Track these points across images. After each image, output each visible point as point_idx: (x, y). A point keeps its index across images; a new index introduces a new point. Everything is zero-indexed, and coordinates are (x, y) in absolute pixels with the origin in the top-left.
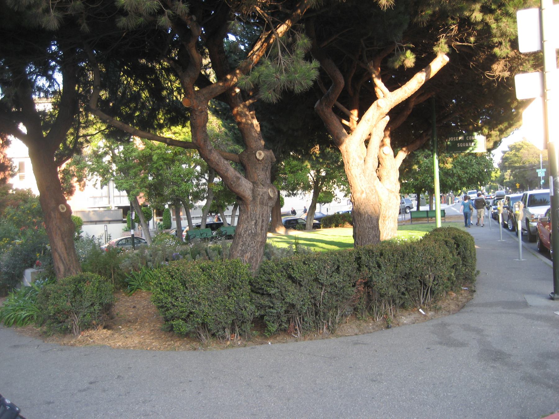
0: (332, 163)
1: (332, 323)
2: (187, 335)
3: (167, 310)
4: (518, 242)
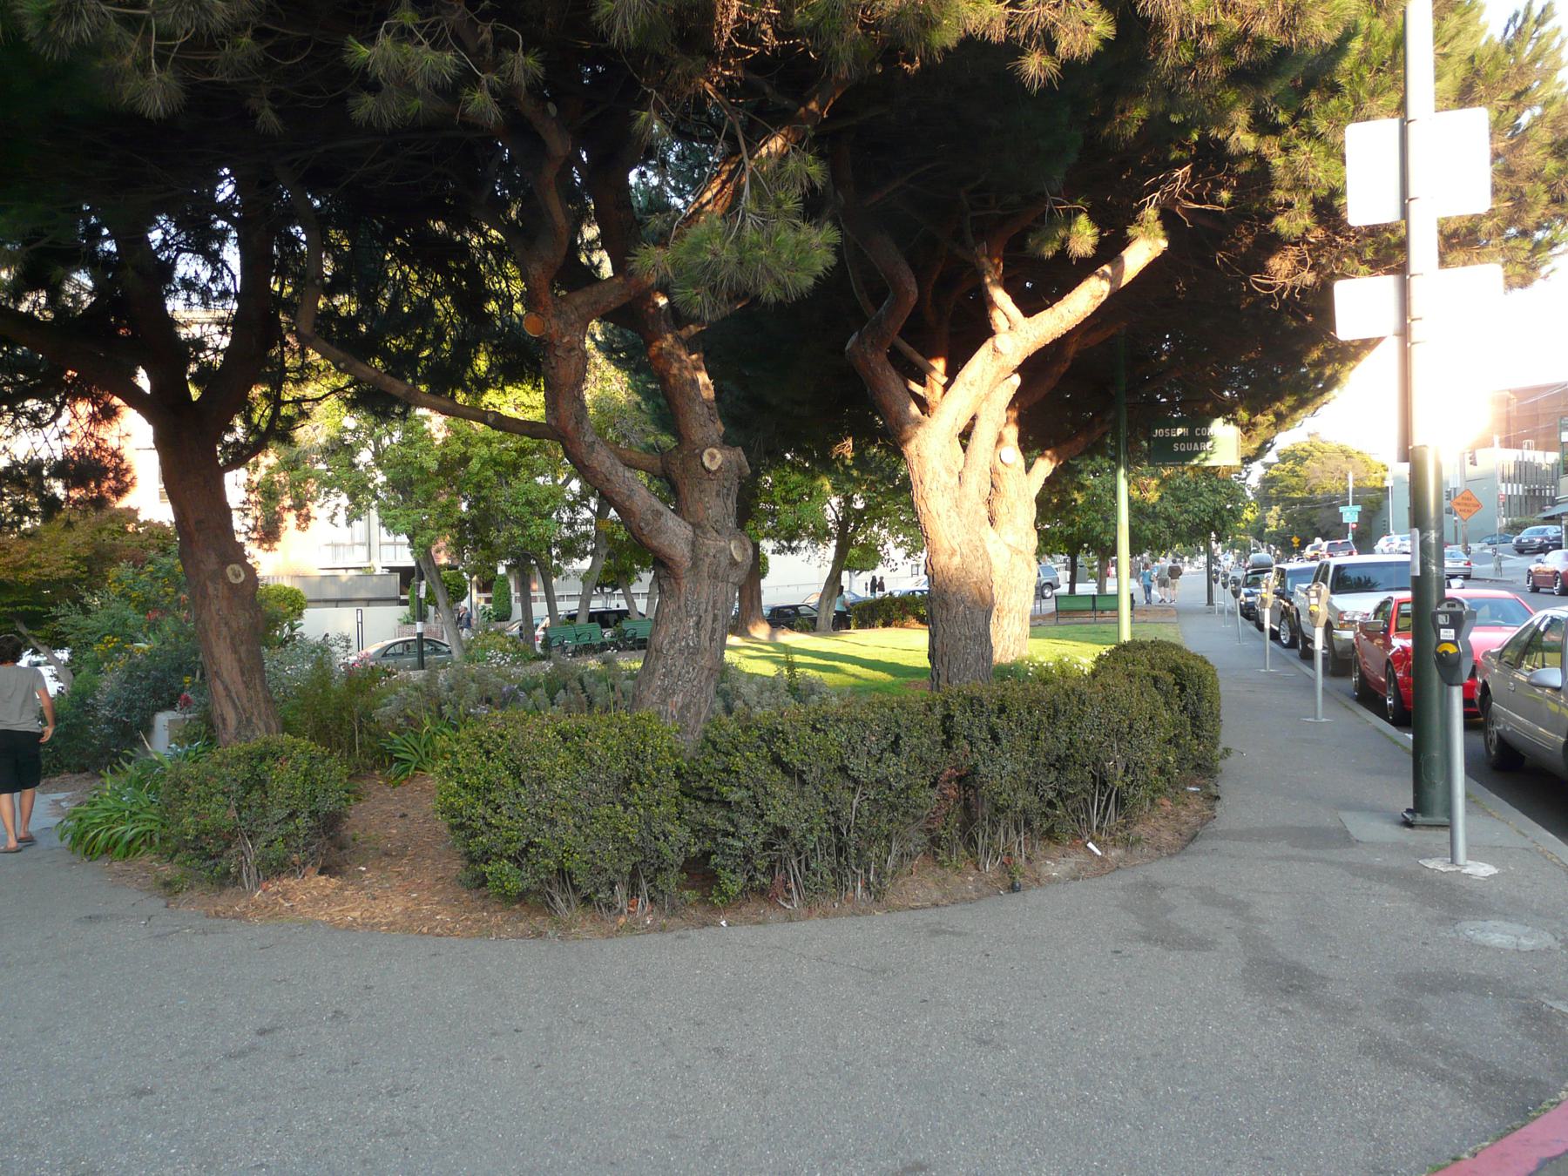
0: (880, 482)
1: (877, 874)
2: (521, 897)
3: (473, 836)
4: (1314, 680)
